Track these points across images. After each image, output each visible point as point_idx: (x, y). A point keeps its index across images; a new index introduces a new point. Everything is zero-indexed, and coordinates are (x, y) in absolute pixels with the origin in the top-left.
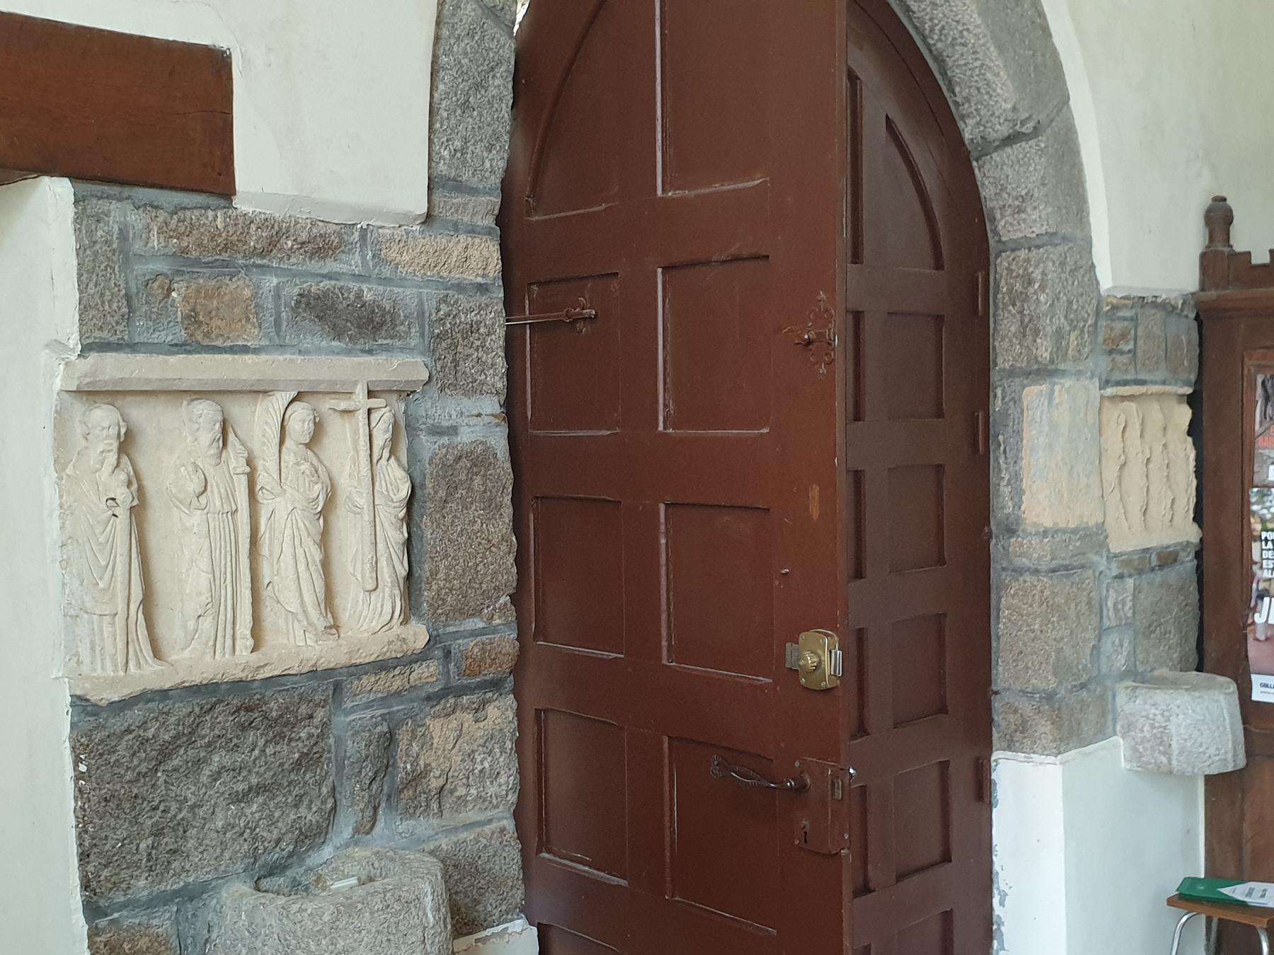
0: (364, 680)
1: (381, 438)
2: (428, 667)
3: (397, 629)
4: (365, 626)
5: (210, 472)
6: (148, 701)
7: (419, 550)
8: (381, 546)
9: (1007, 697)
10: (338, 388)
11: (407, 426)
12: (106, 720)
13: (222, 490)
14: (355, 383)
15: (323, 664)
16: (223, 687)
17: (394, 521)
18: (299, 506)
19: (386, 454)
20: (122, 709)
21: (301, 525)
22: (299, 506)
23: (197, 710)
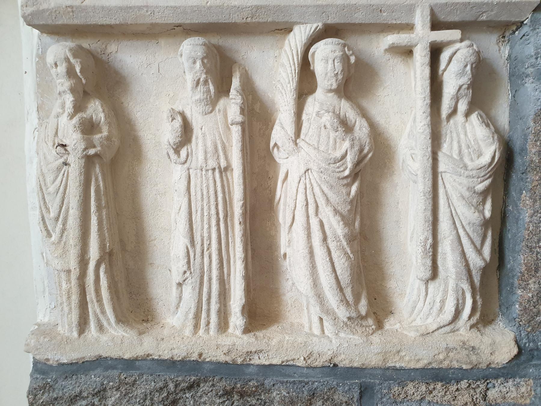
0: (410, 388)
1: (453, 80)
2: (517, 386)
3: (464, 331)
4: (418, 322)
5: (197, 120)
6: (107, 369)
7: (515, 235)
8: (444, 225)
9: (86, 22)
10: (385, 17)
11: (511, 75)
12: (56, 381)
13: (209, 144)
14: (411, 9)
15: (343, 361)
16: (206, 366)
17: (467, 194)
18: (315, 168)
19: (462, 106)
20: (74, 373)
21: (317, 190)
22: (315, 168)
23: (171, 386)
